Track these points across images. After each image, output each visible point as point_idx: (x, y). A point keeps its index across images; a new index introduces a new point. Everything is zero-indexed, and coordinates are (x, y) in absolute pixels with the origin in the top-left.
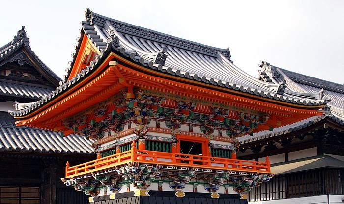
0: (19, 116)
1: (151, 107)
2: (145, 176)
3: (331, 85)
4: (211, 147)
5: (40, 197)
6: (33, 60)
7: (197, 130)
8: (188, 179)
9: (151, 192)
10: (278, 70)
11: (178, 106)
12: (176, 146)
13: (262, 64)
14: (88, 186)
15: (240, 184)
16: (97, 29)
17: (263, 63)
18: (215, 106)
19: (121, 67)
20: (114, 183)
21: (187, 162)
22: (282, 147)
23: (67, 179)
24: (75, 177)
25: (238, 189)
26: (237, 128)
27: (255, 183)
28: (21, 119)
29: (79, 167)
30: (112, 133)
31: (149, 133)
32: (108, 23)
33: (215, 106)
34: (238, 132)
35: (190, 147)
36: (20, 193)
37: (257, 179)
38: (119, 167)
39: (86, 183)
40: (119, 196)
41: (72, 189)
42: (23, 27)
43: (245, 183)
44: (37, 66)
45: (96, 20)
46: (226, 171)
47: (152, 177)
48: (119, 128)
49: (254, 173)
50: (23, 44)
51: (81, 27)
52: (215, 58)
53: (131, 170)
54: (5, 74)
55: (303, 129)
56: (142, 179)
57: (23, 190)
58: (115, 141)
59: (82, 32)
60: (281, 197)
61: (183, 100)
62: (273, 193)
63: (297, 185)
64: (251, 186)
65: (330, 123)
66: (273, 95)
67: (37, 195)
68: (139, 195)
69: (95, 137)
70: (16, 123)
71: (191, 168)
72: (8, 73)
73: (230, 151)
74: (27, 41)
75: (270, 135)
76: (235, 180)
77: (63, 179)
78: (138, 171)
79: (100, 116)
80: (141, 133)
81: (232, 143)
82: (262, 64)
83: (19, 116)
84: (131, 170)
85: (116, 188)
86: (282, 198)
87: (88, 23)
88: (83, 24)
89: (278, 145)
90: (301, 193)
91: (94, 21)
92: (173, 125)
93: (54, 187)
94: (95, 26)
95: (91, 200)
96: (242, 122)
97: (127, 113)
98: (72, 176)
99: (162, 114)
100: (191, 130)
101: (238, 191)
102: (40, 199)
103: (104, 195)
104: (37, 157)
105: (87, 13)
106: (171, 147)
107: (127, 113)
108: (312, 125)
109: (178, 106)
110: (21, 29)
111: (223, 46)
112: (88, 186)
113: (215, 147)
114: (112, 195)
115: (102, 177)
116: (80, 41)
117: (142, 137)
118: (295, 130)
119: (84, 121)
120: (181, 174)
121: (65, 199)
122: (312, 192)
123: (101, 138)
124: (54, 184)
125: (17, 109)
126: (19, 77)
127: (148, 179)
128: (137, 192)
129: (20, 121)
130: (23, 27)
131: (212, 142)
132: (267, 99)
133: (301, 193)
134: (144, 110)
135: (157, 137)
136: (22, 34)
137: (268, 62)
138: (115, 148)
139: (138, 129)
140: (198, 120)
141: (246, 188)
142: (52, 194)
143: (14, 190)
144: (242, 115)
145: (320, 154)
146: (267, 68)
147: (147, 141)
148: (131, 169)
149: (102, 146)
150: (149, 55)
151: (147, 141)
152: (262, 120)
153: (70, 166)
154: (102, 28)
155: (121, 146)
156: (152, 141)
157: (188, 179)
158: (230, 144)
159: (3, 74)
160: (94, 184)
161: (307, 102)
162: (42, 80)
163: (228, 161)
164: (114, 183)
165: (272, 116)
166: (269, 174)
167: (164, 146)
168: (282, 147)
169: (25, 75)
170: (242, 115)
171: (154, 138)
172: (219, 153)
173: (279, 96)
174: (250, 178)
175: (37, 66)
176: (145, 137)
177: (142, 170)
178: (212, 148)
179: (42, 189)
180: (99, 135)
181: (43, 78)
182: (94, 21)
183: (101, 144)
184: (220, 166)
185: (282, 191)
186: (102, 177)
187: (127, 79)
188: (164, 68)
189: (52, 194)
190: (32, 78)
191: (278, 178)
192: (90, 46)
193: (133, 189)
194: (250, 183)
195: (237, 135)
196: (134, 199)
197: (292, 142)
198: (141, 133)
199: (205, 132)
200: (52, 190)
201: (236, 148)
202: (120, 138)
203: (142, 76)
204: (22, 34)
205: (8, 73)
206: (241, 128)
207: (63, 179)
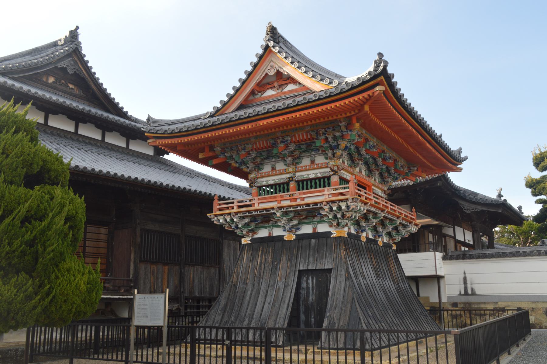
23: (216, 216)
24: (236, 213)
42: (77, 28)
54: (47, 79)
58: (288, 176)
59: (266, 48)
72: (51, 80)
129: (154, 140)
130: (77, 28)
136: (74, 35)
149: (259, 180)
155: (298, 182)
159: (44, 79)
169: (71, 86)
196: (329, 240)
202: (295, 172)
204: (74, 35)
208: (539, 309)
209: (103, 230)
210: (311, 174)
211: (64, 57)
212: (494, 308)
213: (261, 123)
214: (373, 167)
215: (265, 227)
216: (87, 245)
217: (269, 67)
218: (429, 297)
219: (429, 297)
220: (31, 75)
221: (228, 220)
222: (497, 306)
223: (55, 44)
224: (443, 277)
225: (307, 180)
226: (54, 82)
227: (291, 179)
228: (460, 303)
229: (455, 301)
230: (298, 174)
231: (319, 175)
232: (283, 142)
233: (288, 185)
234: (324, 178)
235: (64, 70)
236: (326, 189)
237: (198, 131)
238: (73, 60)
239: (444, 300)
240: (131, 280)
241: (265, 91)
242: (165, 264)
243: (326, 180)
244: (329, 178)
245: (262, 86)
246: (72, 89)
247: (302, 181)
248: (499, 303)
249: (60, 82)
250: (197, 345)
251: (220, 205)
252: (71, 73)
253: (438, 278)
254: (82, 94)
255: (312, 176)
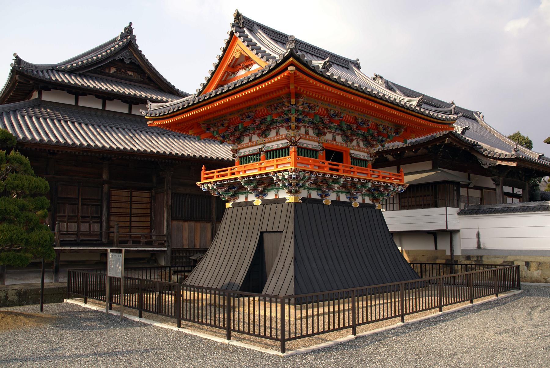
0: (151, 116)
1: (307, 115)
2: (301, 183)
3: (434, 101)
4: (351, 156)
5: (151, 202)
6: (140, 58)
7: (339, 139)
8: (336, 187)
9: (303, 199)
10: (390, 84)
11: (328, 115)
12: (322, 154)
13: (374, 77)
14: (227, 192)
15: (376, 194)
16: (247, 32)
17: (376, 76)
18: (360, 116)
19: (298, 73)
20: (260, 189)
21: (337, 170)
22: (394, 159)
23: (203, 184)
24: (215, 182)
25: (374, 198)
26: (374, 139)
27: (390, 193)
28: (154, 120)
29: (218, 172)
30: (255, 138)
31: (301, 141)
32: (255, 26)
33: (360, 116)
34: (375, 143)
35: (335, 156)
36: (131, 197)
37: (394, 189)
38: (275, 172)
39: (226, 188)
40: (266, 203)
41: (207, 194)
42: (131, 24)
43: (381, 193)
44: (143, 65)
45: (245, 23)
46: (369, 180)
47: (307, 183)
48: (264, 134)
49: (392, 184)
50: (130, 41)
51: (230, 29)
52: (348, 69)
53: (290, 177)
54: (110, 71)
55: (424, 143)
56: (294, 185)
57: (135, 194)
58: (260, 147)
59: (232, 34)
60: (388, 209)
61: (334, 109)
62: (386, 204)
63: (413, 197)
64: (386, 196)
65: (451, 138)
66: (413, 107)
67: (148, 200)
68: (293, 201)
69: (234, 142)
70: (148, 123)
71: (341, 176)
72: (113, 70)
73: (366, 161)
74: (133, 38)
75: (388, 147)
76: (375, 191)
77: (198, 183)
78: (297, 177)
79: (247, 120)
80: (293, 139)
81: (368, 153)
82: (374, 77)
83: (151, 116)
84: (290, 177)
85: (260, 195)
86: (390, 210)
87: (237, 25)
88: (233, 26)
89: (390, 157)
90: (410, 206)
91: (242, 24)
92: (320, 133)
93: (170, 192)
94: (245, 29)
95: (229, 205)
96: (379, 133)
97: (281, 119)
98: (208, 182)
99: (312, 122)
100: (334, 139)
101: (373, 201)
102: (151, 204)
103: (274, 198)
104: (164, 161)
105: (237, 16)
106: (318, 155)
107: (281, 119)
108: (436, 140)
109: (328, 115)
110: (128, 25)
111: (354, 59)
112: (227, 192)
113: (355, 156)
114: (257, 202)
115: (249, 182)
116: (228, 43)
117: (294, 143)
118: (415, 144)
119: (226, 125)
120: (330, 182)
121: (179, 204)
122: (421, 205)
123: (240, 143)
124: (170, 189)
125: (149, 109)
126: (123, 76)
127: (304, 185)
128: (290, 199)
129: (152, 122)
130: (131, 24)
131: (352, 151)
132: (408, 111)
133: (417, 205)
134: (300, 117)
135: (307, 144)
136: (129, 31)
137: (381, 75)
138: (259, 154)
139: (290, 136)
140: (341, 130)
141: (381, 198)
142: (167, 199)
143: (125, 193)
144: (381, 127)
145: (434, 168)
146: (380, 81)
147: (298, 148)
148: (291, 176)
149: (241, 151)
150: (318, 63)
151: (298, 148)
152: (397, 133)
153: (206, 170)
154: (251, 31)
155: (267, 152)
156: (302, 148)
157: (336, 187)
158: (366, 154)
159: (107, 71)
160: (235, 188)
161: (452, 118)
162: (146, 80)
163: (358, 169)
164: (260, 189)
165: (406, 130)
166: (403, 185)
167: (312, 153)
168: (394, 159)
169: (130, 73)
170: (381, 127)
171: (305, 146)
172: (356, 161)
173: (418, 109)
174: (386, 188)
175: (143, 65)
176: (297, 144)
177: (301, 177)
178: (352, 158)
179: (153, 194)
180: (238, 140)
181: (149, 78)
182: (242, 24)
183: (239, 149)
184: (364, 176)
185: (390, 204)
186: (249, 182)
187: (296, 86)
188: (327, 74)
189: (167, 199)
190: (138, 77)
191: (413, 188)
192: (239, 49)
193: (283, 194)
194: (387, 193)
195: (373, 146)
196: (285, 206)
197: (405, 155)
198: (293, 139)
199: (346, 142)
200: (167, 194)
201: (371, 159)
202: (265, 143)
203: (311, 82)
204: (129, 31)
205: (113, 70)
206: (378, 139)
207: (198, 183)
208: (546, 263)
209: (146, 194)
210: (274, 145)
211: (121, 50)
212: (504, 262)
213: (217, 104)
214: (349, 132)
215: (272, 190)
216: (133, 207)
217: (235, 51)
218: (445, 250)
219: (445, 250)
220: (96, 68)
221: (211, 188)
222: (506, 260)
223: (114, 40)
224: (457, 231)
225: (273, 150)
226: (115, 72)
227: (260, 150)
228: (473, 257)
229: (469, 255)
230: (267, 145)
231: (281, 146)
232: (248, 117)
233: (288, 150)
234: (285, 148)
235: (122, 61)
236: (275, 159)
237: (175, 113)
238: (128, 52)
239: (458, 252)
240: (165, 235)
241: (237, 71)
242: (197, 221)
243: (287, 150)
244: (288, 148)
245: (235, 66)
246: (131, 75)
247: (270, 151)
248: (509, 257)
249: (120, 71)
250: (164, 295)
251: (207, 174)
252: (129, 62)
253: (451, 234)
254: (140, 79)
255: (275, 147)
